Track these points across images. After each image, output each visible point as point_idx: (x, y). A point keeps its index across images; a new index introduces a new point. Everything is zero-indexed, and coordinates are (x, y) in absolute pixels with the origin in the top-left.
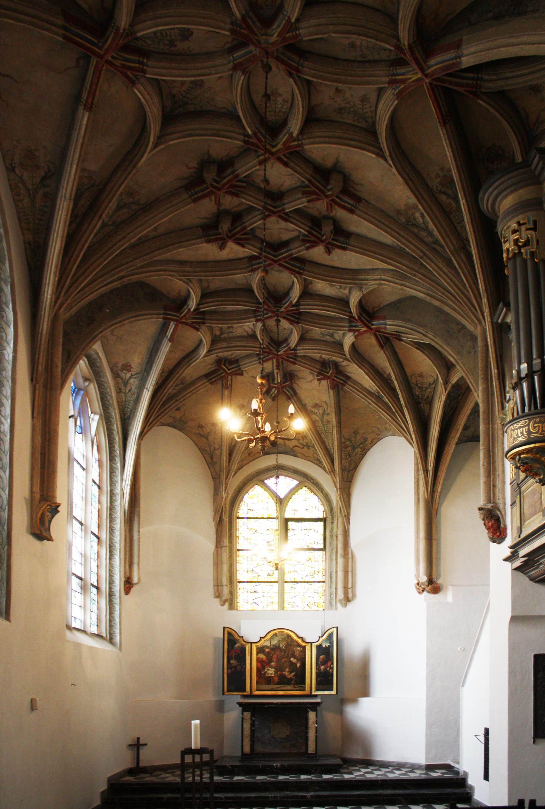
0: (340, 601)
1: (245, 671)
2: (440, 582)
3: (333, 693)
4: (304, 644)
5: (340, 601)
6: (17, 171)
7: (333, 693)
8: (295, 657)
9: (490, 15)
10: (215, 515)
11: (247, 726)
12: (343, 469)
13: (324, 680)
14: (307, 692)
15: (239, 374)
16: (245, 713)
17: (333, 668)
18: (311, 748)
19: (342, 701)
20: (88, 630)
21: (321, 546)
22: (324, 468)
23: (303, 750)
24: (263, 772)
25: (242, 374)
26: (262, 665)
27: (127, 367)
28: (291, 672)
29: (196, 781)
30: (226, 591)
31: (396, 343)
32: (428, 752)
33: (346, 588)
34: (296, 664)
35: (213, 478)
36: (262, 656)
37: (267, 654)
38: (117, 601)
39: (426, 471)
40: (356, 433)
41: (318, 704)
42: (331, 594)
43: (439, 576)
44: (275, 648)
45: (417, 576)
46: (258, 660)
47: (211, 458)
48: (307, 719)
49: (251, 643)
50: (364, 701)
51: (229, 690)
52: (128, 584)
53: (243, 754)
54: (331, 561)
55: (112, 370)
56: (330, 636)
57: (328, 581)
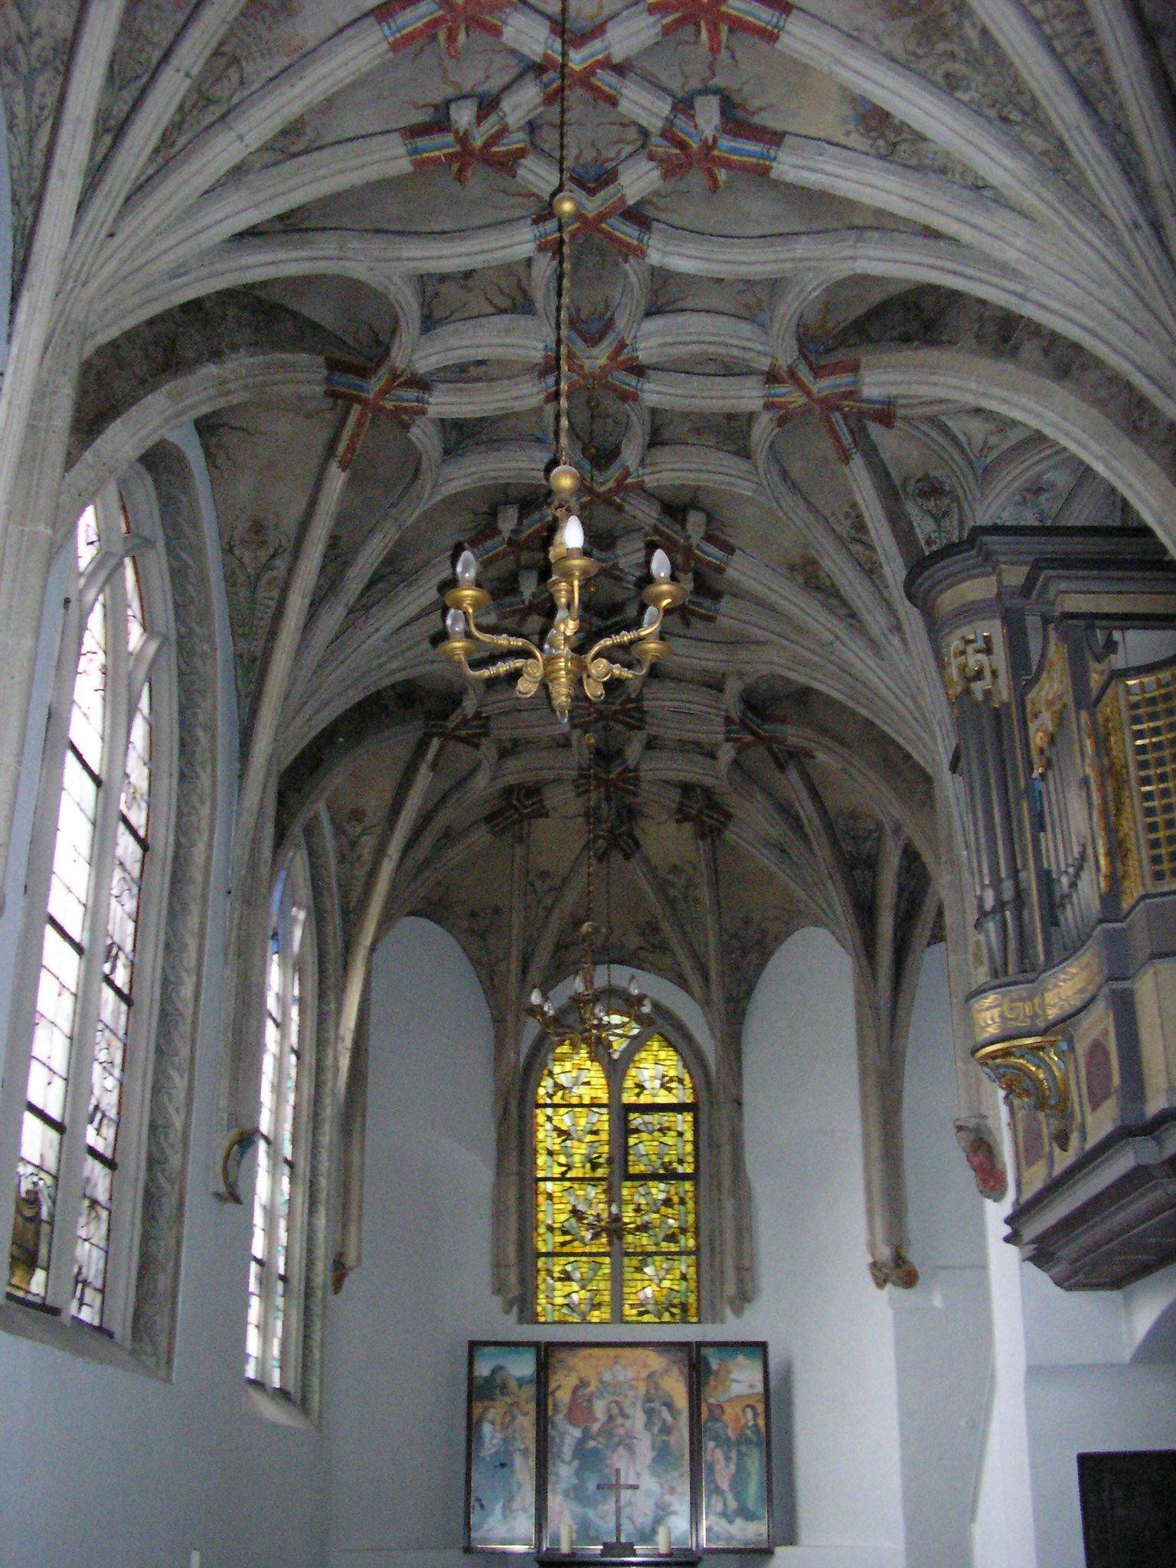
6: (236, 552)
9: (895, 334)
15: (542, 816)
22: (691, 994)
25: (547, 815)
27: (357, 815)
31: (805, 761)
39: (875, 1008)
40: (747, 921)
45: (872, 1246)
52: (340, 1270)
55: (333, 821)
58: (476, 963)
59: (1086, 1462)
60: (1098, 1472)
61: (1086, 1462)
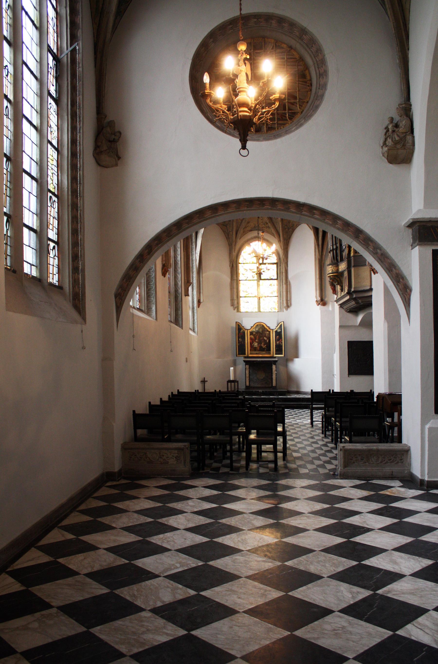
0: (285, 307)
1: (245, 344)
2: (326, 299)
3: (283, 356)
4: (270, 330)
5: (285, 307)
7: (283, 356)
8: (266, 337)
10: (230, 264)
11: (247, 372)
12: (284, 239)
13: (279, 350)
14: (271, 355)
16: (247, 366)
17: (282, 343)
18: (274, 384)
19: (287, 360)
20: (135, 306)
21: (276, 278)
23: (270, 386)
24: (255, 394)
26: (252, 341)
28: (264, 345)
29: (239, 390)
30: (236, 302)
32: (323, 386)
33: (287, 300)
34: (266, 341)
35: (229, 245)
36: (252, 337)
37: (254, 335)
38: (195, 311)
41: (276, 361)
42: (281, 303)
43: (325, 297)
44: (258, 332)
45: (316, 297)
46: (251, 339)
47: (228, 235)
48: (272, 369)
49: (247, 330)
50: (296, 360)
51: (239, 354)
52: (199, 302)
53: (246, 386)
54: (280, 285)
56: (281, 326)
57: (279, 296)
58: (224, 232)
59: (349, 342)
60: (351, 344)
61: (349, 342)
